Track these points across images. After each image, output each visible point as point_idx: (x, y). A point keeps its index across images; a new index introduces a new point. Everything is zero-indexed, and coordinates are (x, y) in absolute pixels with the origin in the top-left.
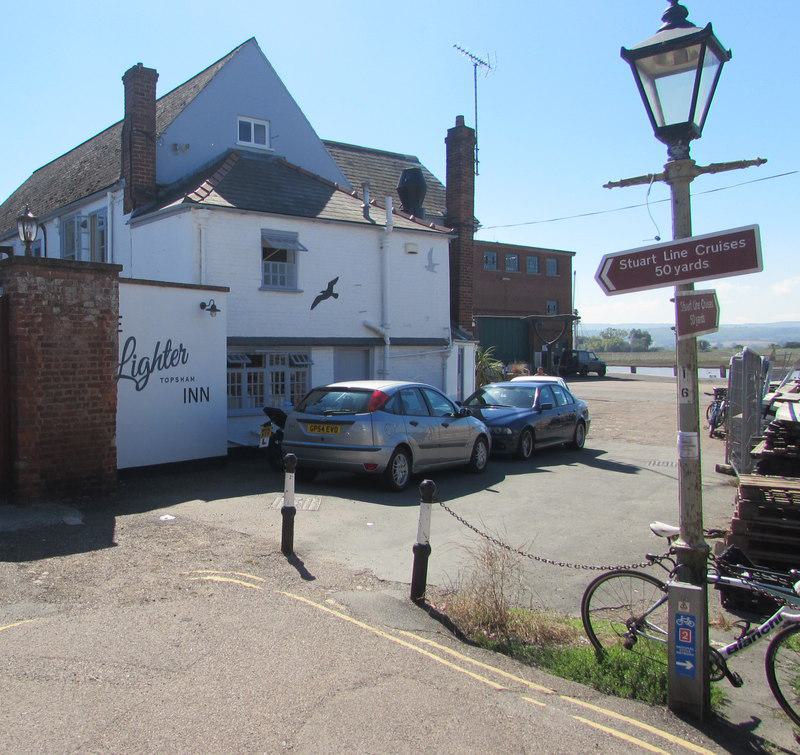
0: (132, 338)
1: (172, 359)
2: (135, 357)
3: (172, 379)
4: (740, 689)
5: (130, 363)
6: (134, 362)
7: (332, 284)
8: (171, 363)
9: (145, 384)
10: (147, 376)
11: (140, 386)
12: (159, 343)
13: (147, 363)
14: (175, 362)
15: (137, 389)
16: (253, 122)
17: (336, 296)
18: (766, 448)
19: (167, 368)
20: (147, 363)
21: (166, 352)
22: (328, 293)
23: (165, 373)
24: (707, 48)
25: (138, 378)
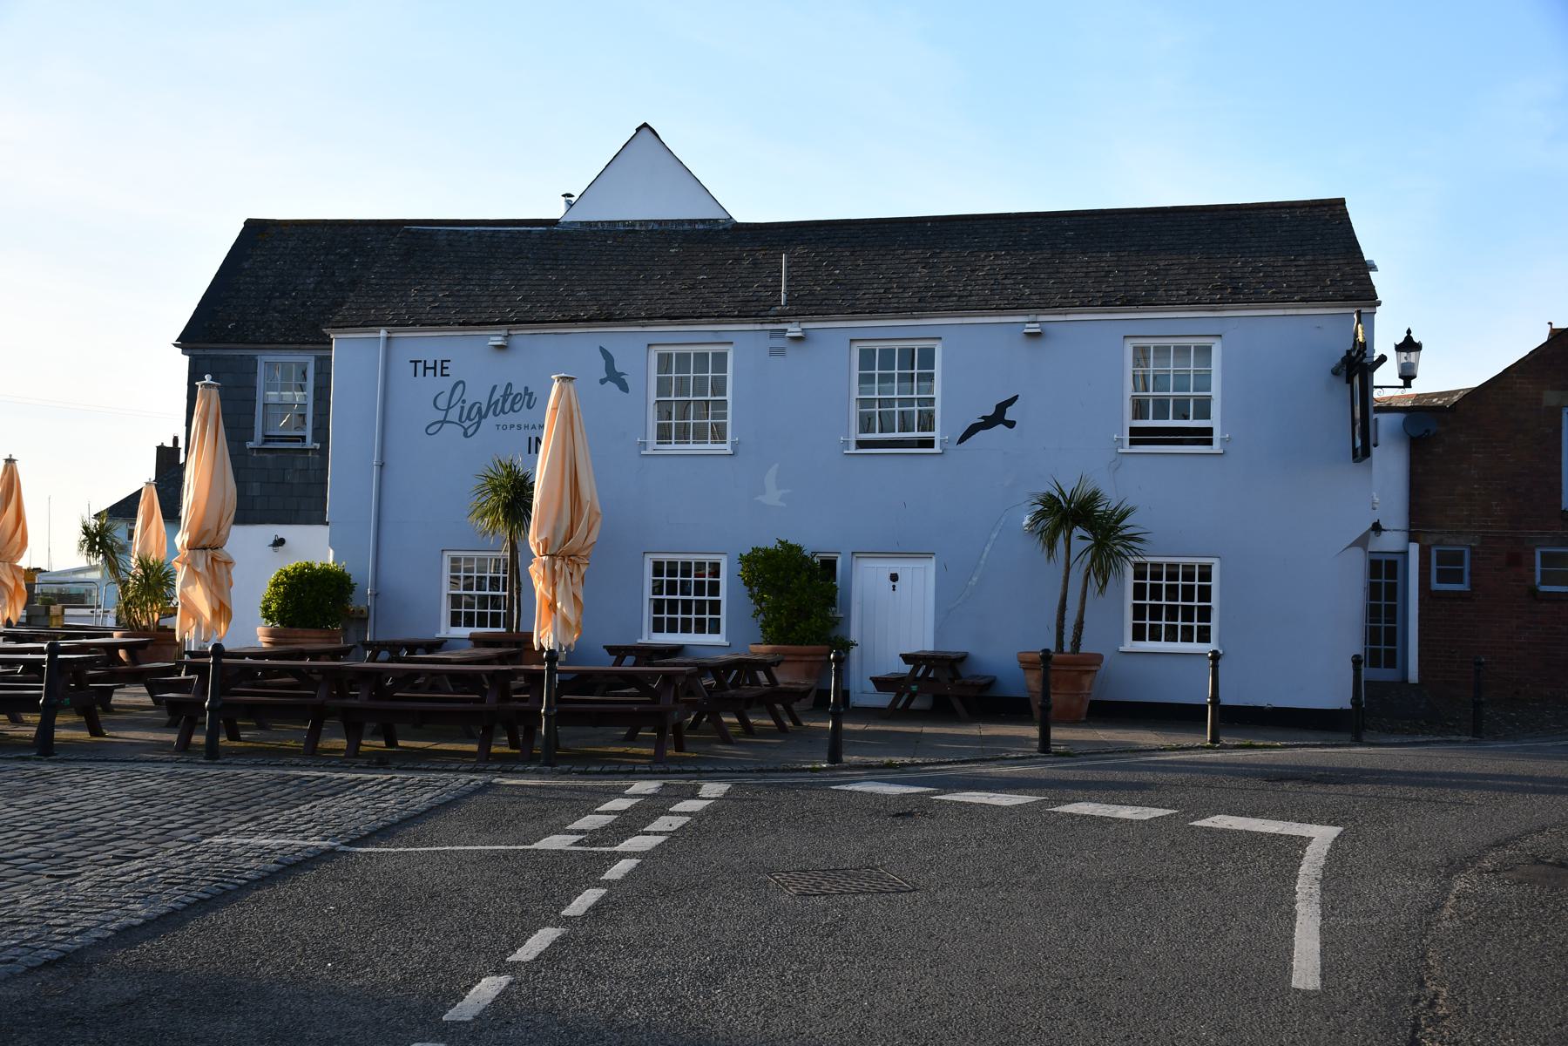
0: (463, 382)
1: (513, 403)
2: (464, 402)
3: (512, 426)
4: (899, 575)
5: (457, 408)
6: (462, 408)
7: (1002, 408)
8: (512, 409)
9: (476, 431)
10: (479, 423)
11: (470, 432)
12: (495, 387)
13: (480, 409)
14: (517, 407)
15: (466, 435)
16: (1130, 422)
17: (1011, 424)
18: (700, 787)
19: (504, 413)
20: (480, 409)
21: (505, 397)
22: (997, 418)
23: (502, 419)
24: (604, 891)
25: (467, 424)
